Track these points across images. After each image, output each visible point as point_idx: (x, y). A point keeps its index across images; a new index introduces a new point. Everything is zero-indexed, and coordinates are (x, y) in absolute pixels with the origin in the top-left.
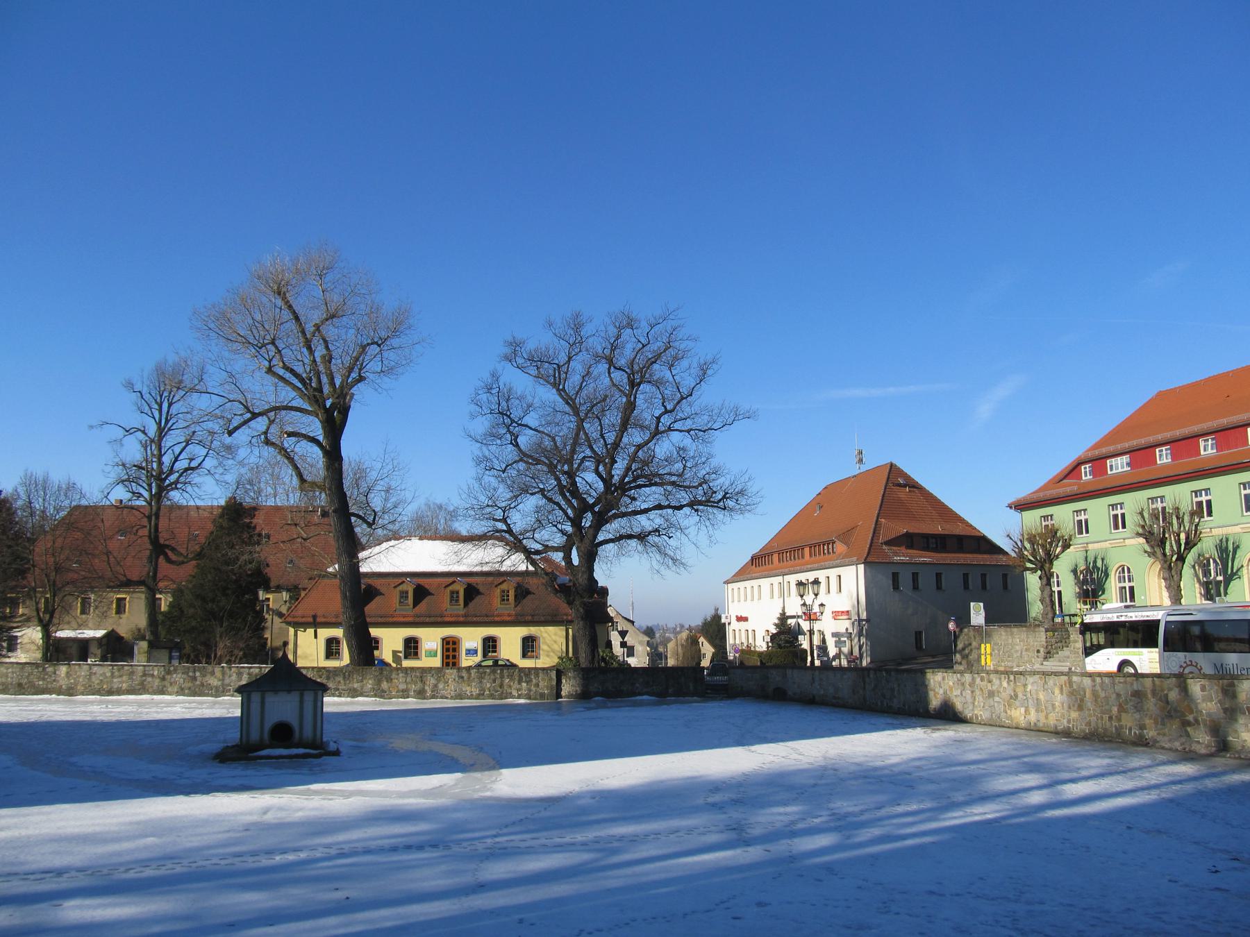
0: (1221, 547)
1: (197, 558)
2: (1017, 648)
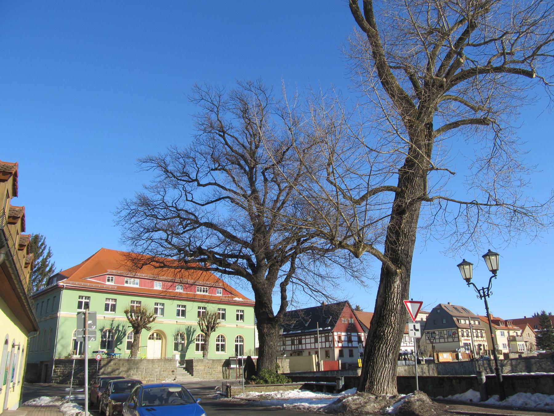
0: (188, 330)
2: (156, 370)
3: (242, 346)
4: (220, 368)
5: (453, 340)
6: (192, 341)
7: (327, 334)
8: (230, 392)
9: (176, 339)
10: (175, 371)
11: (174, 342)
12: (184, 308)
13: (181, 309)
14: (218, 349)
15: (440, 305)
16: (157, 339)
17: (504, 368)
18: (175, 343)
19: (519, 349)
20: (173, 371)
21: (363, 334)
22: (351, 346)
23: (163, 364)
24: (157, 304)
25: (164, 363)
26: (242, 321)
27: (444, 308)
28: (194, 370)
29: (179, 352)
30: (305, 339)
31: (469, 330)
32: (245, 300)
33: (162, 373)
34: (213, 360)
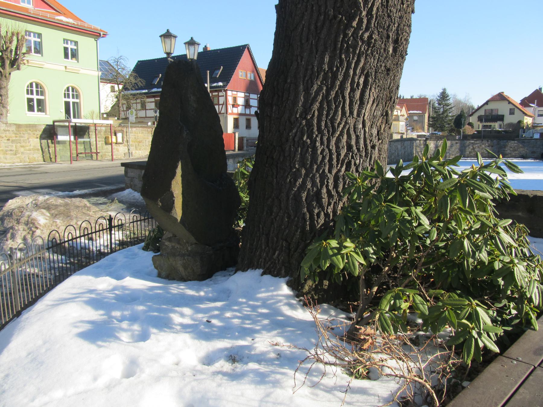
4: (35, 142)
7: (216, 94)
14: (31, 108)
22: (249, 113)
26: (74, 60)
32: (79, 23)
34: (19, 126)
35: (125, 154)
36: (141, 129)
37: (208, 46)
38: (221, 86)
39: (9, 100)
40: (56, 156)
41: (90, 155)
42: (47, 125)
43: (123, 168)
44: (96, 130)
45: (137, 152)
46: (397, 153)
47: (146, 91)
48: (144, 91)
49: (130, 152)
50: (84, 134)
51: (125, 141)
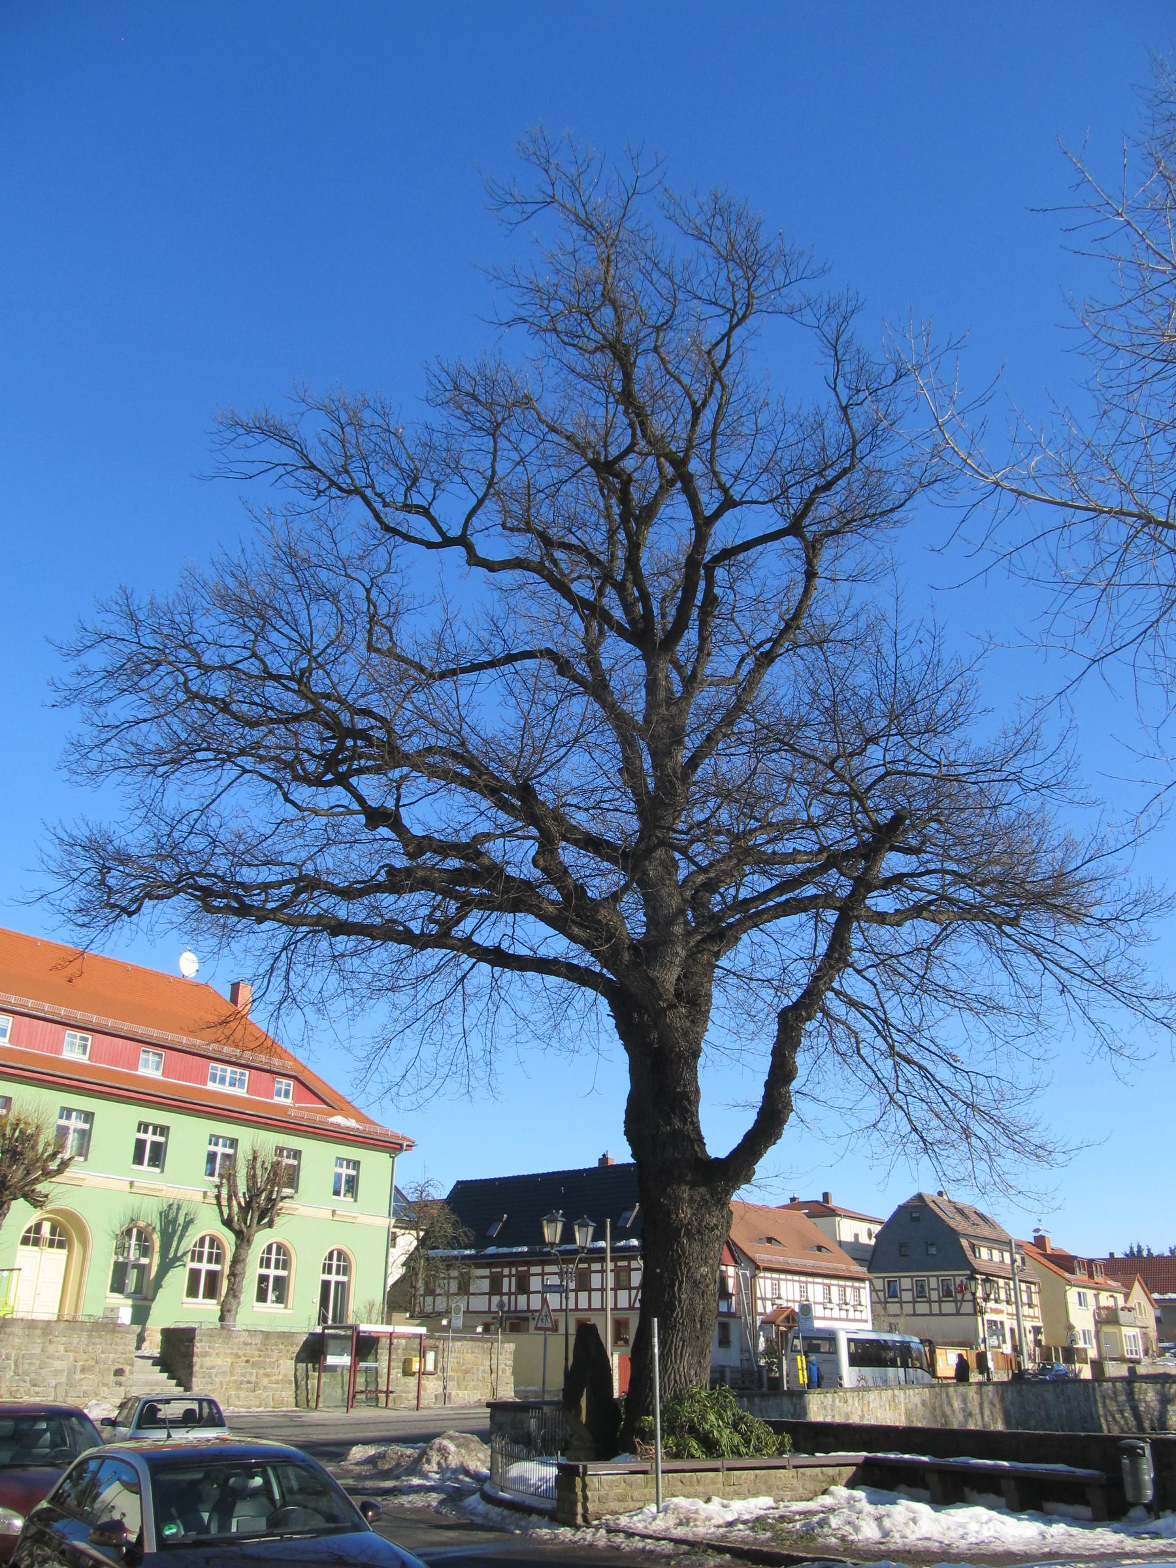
0: (167, 1217)
1: (82, 920)
2: (58, 1364)
3: (342, 1287)
4: (287, 1366)
5: (958, 1310)
6: (177, 1259)
7: (625, 1263)
8: (585, 1498)
9: (121, 1248)
10: (127, 1368)
11: (114, 1258)
12: (161, 1134)
13: (150, 1137)
15: (920, 1197)
16: (51, 1244)
17: (1169, 1408)
18: (116, 1264)
19: (1127, 1349)
20: (119, 1372)
21: (731, 1271)
23: (84, 1339)
24: (67, 1112)
25: (90, 1337)
27: (932, 1205)
28: (196, 1368)
29: (128, 1297)
30: (543, 1274)
31: (1011, 1283)
32: (368, 1127)
33: (78, 1376)
34: (267, 1335)
35: (436, 1396)
36: (471, 1343)
37: (609, 1156)
38: (634, 1247)
39: (245, 1282)
40: (318, 1396)
41: (373, 1397)
42: (311, 1334)
43: (489, 1410)
44: (391, 1344)
45: (460, 1393)
46: (1043, 1413)
47: (473, 1252)
48: (467, 1252)
49: (448, 1392)
50: (369, 1353)
51: (440, 1369)
